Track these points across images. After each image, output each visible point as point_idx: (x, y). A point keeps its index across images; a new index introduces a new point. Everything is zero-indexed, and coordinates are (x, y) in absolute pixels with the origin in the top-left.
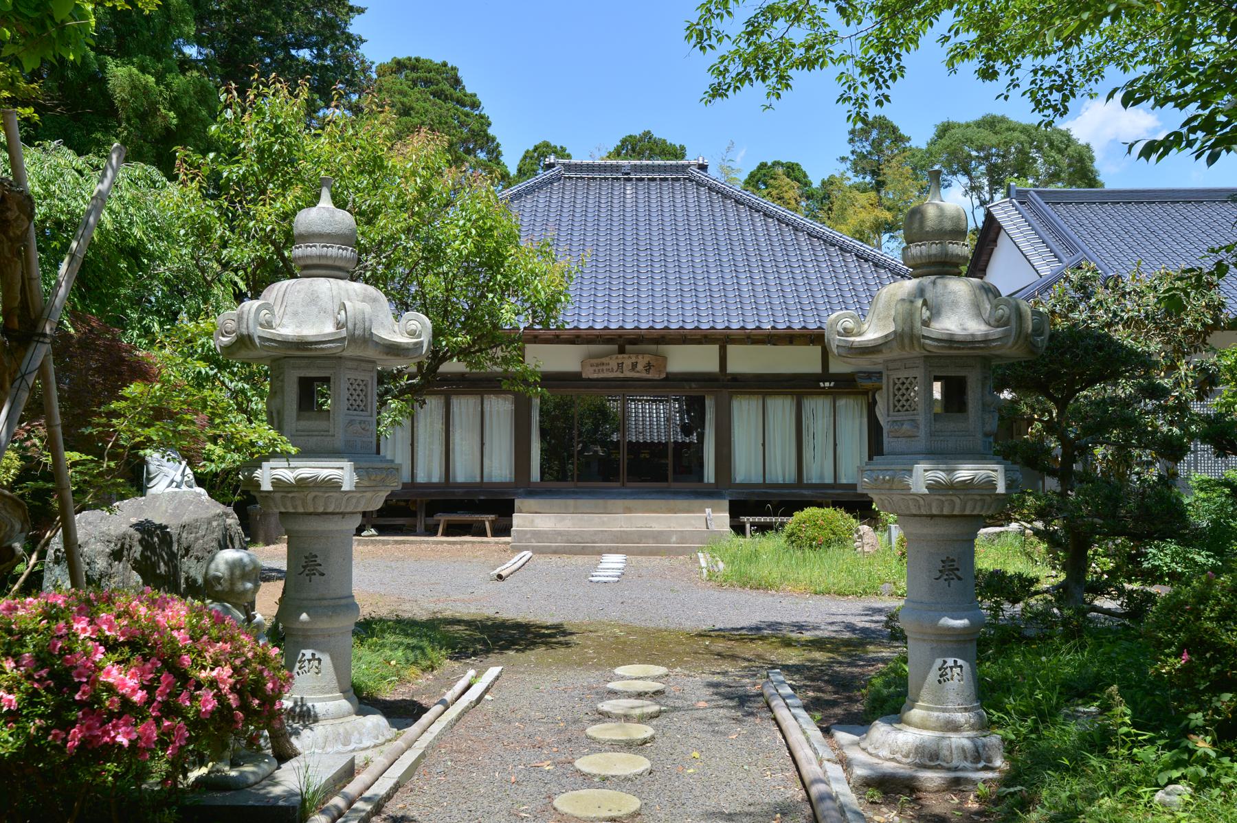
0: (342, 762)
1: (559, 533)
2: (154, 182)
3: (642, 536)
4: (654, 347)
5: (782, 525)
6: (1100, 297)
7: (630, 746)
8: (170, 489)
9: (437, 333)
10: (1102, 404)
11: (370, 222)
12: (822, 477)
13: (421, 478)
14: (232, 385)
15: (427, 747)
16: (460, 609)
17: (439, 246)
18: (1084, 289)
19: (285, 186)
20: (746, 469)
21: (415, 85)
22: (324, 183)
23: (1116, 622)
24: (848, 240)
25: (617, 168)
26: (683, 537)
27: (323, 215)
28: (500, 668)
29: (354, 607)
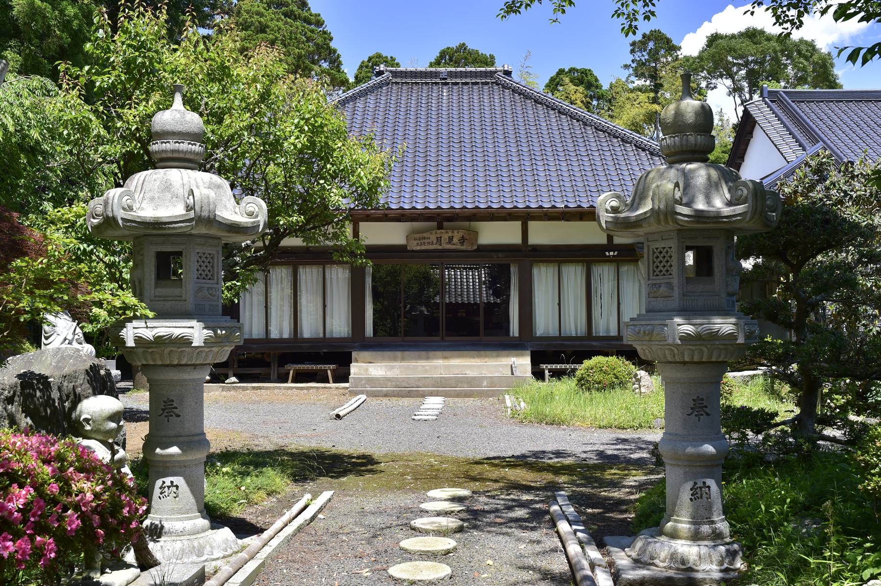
0: (194, 570)
1: (389, 380)
2: (49, 91)
3: (459, 381)
4: (467, 223)
5: (574, 370)
6: (835, 179)
7: (432, 556)
8: (64, 346)
9: (273, 213)
10: (832, 267)
11: (220, 121)
12: (608, 330)
13: (274, 334)
14: (106, 259)
15: (267, 558)
16: (302, 443)
17: (277, 141)
18: (820, 172)
19: (148, 93)
20: (545, 323)
21: (270, 7)
22: (178, 89)
23: (837, 448)
24: (628, 133)
25: (436, 75)
26: (492, 381)
27: (177, 116)
28: (332, 492)
29: (207, 443)
